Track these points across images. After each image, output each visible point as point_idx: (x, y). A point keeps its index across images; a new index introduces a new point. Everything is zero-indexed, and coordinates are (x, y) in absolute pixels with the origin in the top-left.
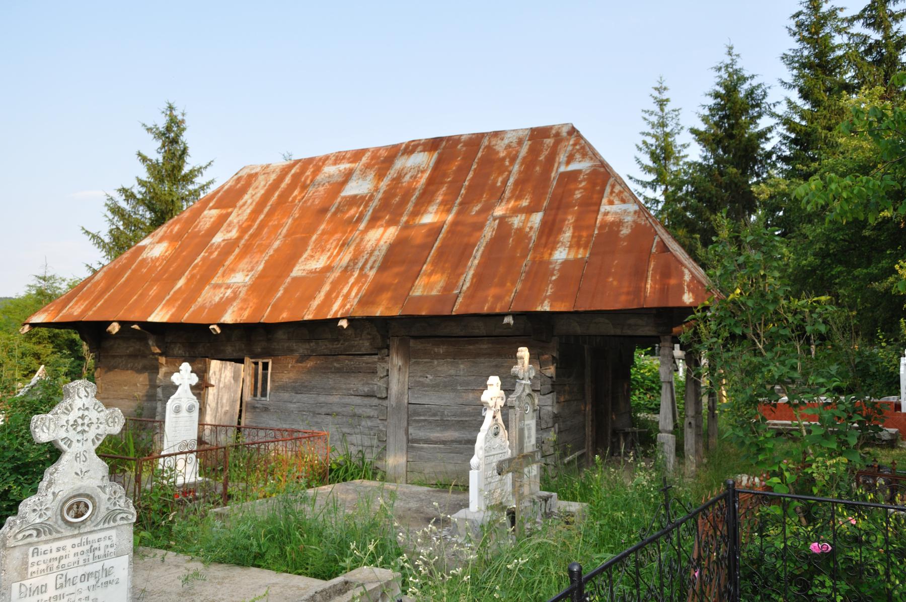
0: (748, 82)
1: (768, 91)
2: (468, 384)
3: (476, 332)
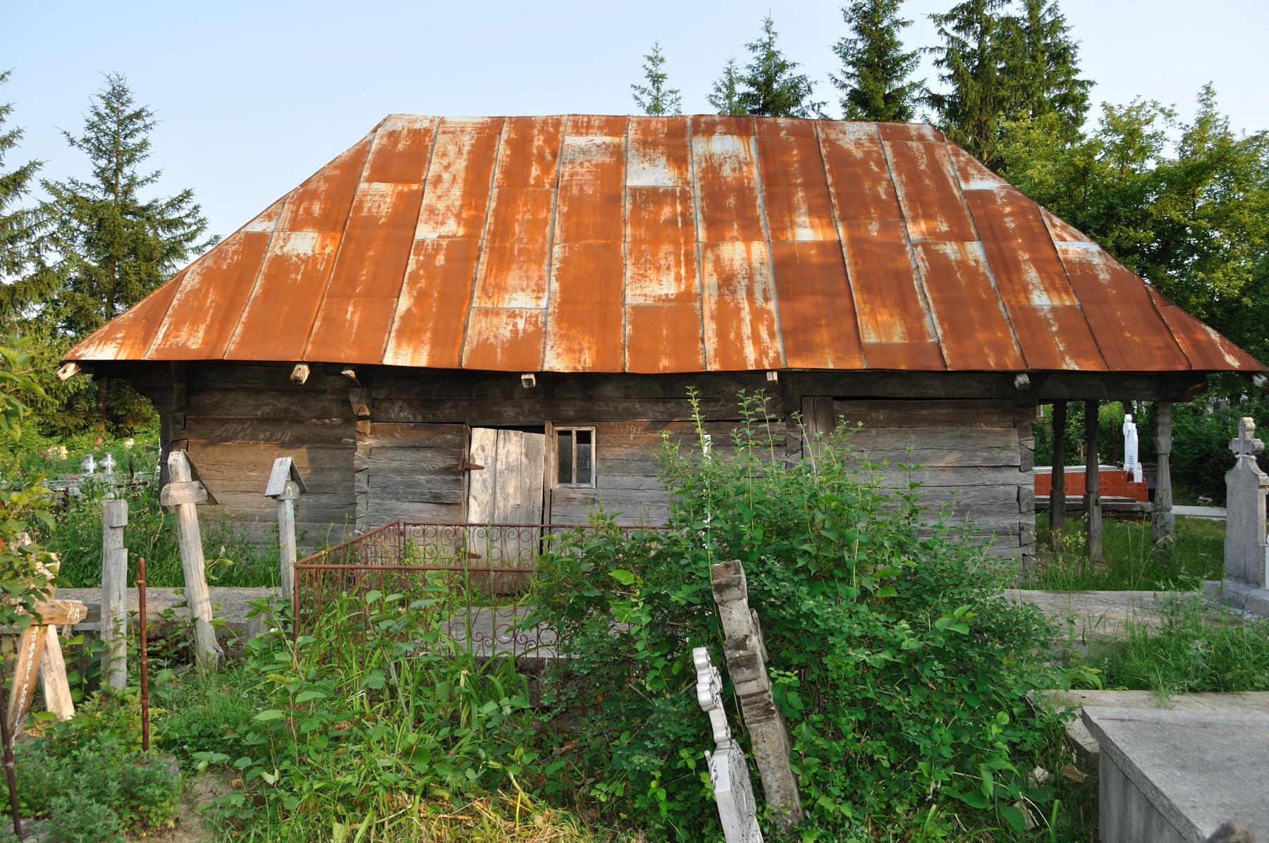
0: (788, 71)
1: (813, 87)
2: (924, 459)
3: (930, 392)
